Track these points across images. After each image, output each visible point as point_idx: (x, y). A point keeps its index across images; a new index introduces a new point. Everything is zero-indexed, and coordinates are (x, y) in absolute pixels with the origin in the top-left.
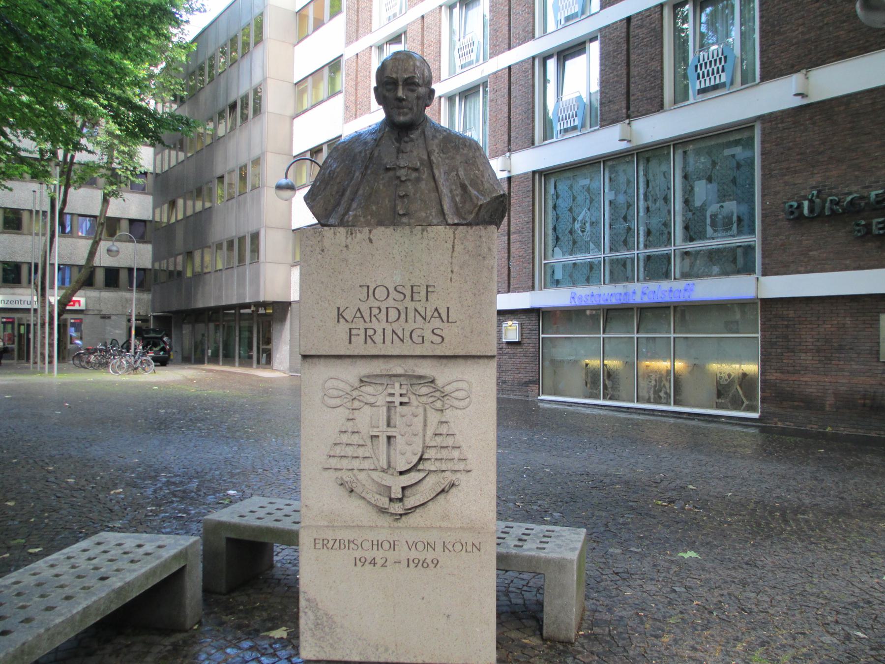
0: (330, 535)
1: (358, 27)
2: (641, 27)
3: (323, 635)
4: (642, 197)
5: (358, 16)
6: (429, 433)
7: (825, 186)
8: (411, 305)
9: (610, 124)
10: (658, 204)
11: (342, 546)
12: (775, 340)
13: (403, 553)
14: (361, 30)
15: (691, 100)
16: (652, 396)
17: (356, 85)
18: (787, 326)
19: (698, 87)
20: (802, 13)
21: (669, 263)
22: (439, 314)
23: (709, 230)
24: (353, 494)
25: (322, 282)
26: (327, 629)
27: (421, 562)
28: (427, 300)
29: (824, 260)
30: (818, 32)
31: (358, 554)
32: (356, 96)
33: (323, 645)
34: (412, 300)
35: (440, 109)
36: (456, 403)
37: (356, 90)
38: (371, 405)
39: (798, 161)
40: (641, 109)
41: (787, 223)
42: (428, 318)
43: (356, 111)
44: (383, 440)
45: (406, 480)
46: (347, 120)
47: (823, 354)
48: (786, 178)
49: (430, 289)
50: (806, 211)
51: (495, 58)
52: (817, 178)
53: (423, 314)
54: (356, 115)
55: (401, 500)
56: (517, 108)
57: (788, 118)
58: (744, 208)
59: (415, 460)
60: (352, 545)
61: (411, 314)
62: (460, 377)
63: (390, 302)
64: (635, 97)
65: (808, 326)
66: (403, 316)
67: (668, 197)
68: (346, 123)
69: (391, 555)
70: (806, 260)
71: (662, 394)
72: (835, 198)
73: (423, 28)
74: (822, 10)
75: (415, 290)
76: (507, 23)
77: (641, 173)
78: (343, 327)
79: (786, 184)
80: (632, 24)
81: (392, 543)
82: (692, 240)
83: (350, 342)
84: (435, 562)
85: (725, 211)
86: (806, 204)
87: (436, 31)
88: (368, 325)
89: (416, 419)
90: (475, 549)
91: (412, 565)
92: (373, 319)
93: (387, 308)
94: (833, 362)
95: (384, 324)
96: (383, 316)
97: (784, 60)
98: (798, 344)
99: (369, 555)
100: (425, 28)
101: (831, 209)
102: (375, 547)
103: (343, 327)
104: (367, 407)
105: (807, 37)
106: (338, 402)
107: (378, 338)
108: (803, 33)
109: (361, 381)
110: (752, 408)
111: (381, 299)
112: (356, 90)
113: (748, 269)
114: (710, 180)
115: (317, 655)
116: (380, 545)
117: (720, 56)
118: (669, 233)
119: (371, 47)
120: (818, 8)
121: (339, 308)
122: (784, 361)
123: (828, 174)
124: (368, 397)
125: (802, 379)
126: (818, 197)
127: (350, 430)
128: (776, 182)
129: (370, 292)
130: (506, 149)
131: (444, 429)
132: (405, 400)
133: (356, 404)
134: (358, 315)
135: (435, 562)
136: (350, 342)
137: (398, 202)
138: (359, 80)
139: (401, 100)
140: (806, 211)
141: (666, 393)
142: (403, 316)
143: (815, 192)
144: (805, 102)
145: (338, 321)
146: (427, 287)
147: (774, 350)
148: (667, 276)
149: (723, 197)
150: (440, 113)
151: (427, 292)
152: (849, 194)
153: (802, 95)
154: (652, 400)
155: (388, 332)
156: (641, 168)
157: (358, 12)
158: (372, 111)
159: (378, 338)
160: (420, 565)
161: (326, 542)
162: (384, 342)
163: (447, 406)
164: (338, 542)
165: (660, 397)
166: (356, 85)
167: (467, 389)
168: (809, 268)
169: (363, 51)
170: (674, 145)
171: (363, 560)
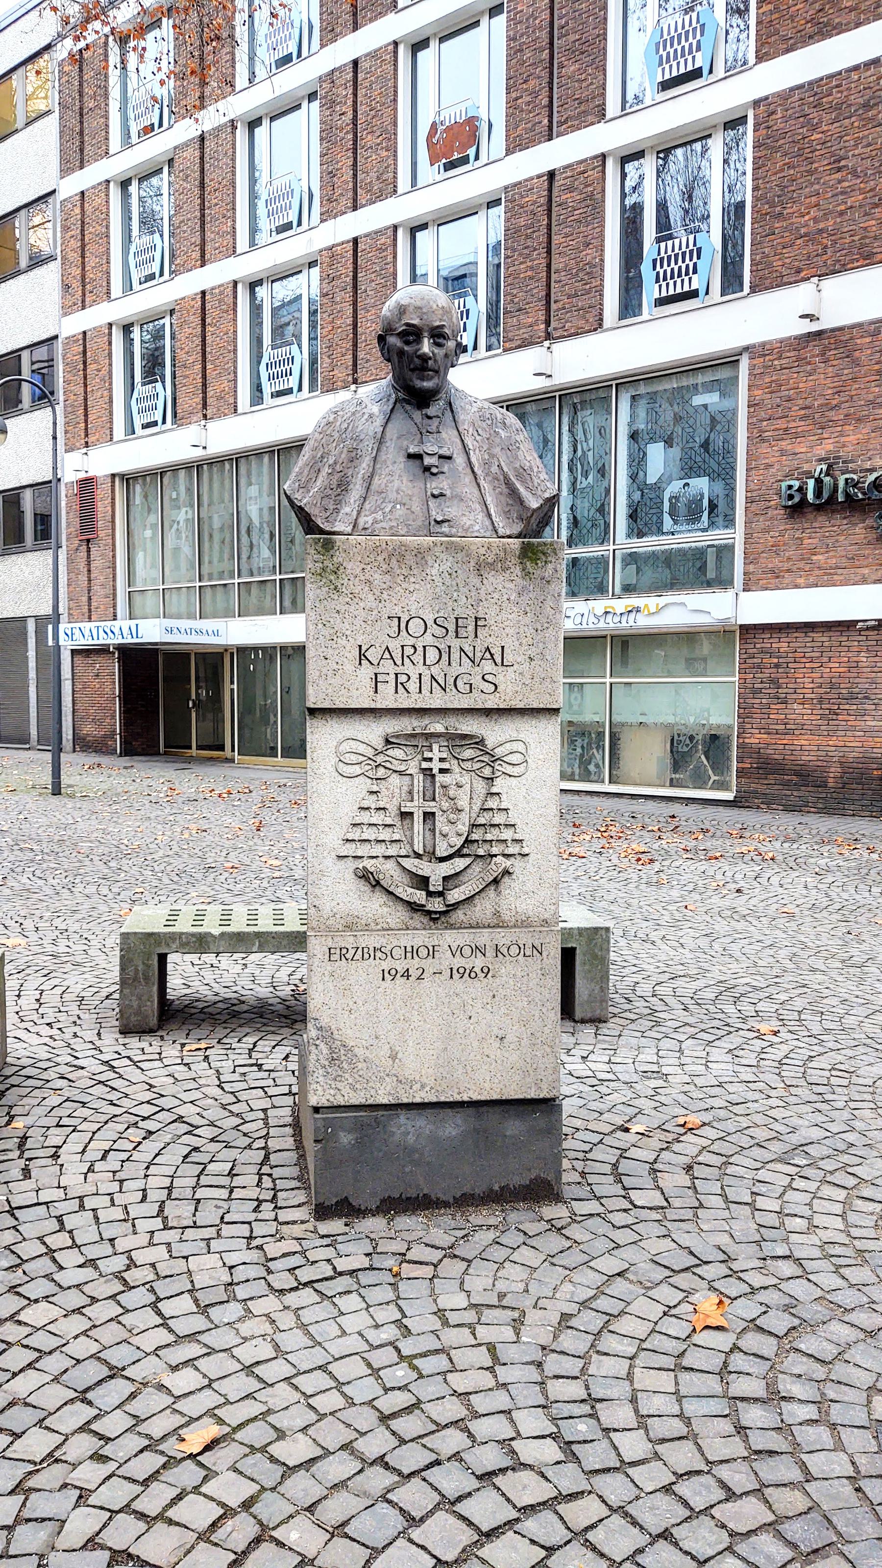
0: (349, 941)
1: (82, 142)
2: (570, 189)
3: (340, 1073)
4: (565, 467)
5: (81, 123)
6: (476, 809)
7: (839, 457)
8: (456, 644)
9: (519, 347)
10: (590, 478)
11: (366, 956)
12: (760, 686)
13: (445, 960)
14: (88, 149)
15: (645, 316)
16: (577, 771)
17: (83, 247)
18: (777, 666)
19: (657, 296)
20: (816, 187)
21: (606, 571)
22: (492, 655)
23: (667, 519)
24: (377, 888)
25: (338, 612)
26: (345, 1065)
27: (468, 971)
28: (476, 636)
29: (831, 568)
30: (838, 220)
31: (386, 965)
32: (83, 269)
33: (340, 1085)
34: (457, 637)
35: (235, 304)
36: (509, 769)
37: (83, 257)
38: (401, 773)
39: (802, 418)
40: (568, 325)
41: (782, 512)
42: (477, 660)
43: (84, 295)
44: (418, 818)
45: (446, 869)
46: (67, 310)
47: (828, 706)
48: (784, 443)
49: (479, 623)
50: (810, 496)
51: (330, 223)
52: (826, 447)
53: (471, 655)
54: (83, 301)
55: (441, 894)
56: (368, 311)
57: (789, 351)
58: (719, 488)
59: (459, 842)
60: (379, 954)
61: (455, 655)
62: (514, 735)
63: (428, 639)
64: (560, 305)
65: (807, 665)
66: (445, 657)
67: (607, 467)
68: (65, 314)
69: (430, 965)
70: (807, 568)
71: (592, 768)
72: (852, 476)
73: (202, 158)
74: (846, 184)
75: (460, 624)
76: (350, 162)
77: (565, 428)
78: (367, 671)
79: (783, 453)
80: (556, 184)
81: (431, 949)
82: (641, 535)
83: (376, 692)
84: (486, 970)
85: (692, 491)
86: (811, 483)
87: (227, 165)
88: (398, 670)
89: (460, 791)
90: (535, 952)
91: (456, 976)
92: (406, 660)
93: (424, 647)
94: (840, 717)
95: (421, 668)
96: (418, 658)
97: (788, 261)
98: (792, 691)
99: (400, 966)
100: (207, 158)
101: (847, 495)
102: (409, 955)
103: (367, 671)
104: (394, 775)
105: (821, 225)
106: (357, 770)
107: (413, 686)
108: (816, 220)
109: (388, 742)
110: (722, 786)
111: (416, 635)
112: (83, 257)
113: (723, 582)
114: (669, 442)
115: (332, 1099)
116: (414, 952)
117: (691, 247)
118: (607, 525)
119: (108, 181)
120: (840, 182)
121: (360, 646)
122: (772, 716)
123: (843, 439)
124: (396, 762)
125: (796, 742)
126: (827, 474)
127: (373, 806)
128: (769, 450)
129: (402, 625)
130: (350, 379)
131: (492, 803)
132: (445, 766)
133: (381, 772)
134: (387, 655)
135: (486, 970)
136: (376, 692)
137: (432, 503)
138: (86, 239)
139: (424, 358)
140: (810, 496)
141: (597, 766)
142: (445, 657)
143: (824, 467)
144: (814, 327)
145: (360, 664)
146: (476, 618)
147: (758, 701)
148: (601, 589)
149: (690, 470)
150: (235, 310)
151: (476, 625)
152: (872, 470)
153: (811, 317)
154: (577, 777)
155: (426, 679)
156: (566, 420)
157: (81, 115)
158: (113, 297)
159: (413, 686)
160: (466, 975)
161: (344, 951)
162: (420, 692)
163: (498, 774)
164: (360, 950)
165: (589, 773)
166: (83, 247)
167: (523, 751)
168: (811, 579)
169: (93, 187)
170: (617, 385)
171: (393, 972)
